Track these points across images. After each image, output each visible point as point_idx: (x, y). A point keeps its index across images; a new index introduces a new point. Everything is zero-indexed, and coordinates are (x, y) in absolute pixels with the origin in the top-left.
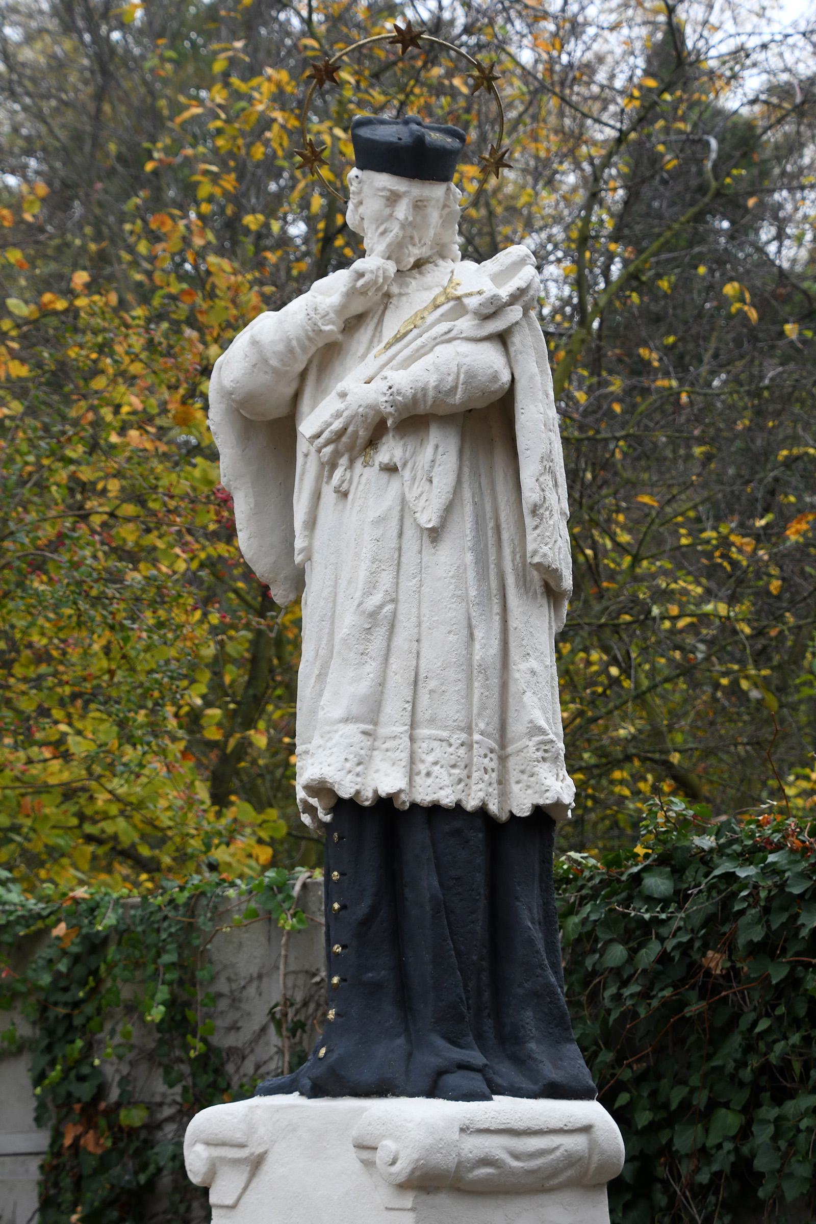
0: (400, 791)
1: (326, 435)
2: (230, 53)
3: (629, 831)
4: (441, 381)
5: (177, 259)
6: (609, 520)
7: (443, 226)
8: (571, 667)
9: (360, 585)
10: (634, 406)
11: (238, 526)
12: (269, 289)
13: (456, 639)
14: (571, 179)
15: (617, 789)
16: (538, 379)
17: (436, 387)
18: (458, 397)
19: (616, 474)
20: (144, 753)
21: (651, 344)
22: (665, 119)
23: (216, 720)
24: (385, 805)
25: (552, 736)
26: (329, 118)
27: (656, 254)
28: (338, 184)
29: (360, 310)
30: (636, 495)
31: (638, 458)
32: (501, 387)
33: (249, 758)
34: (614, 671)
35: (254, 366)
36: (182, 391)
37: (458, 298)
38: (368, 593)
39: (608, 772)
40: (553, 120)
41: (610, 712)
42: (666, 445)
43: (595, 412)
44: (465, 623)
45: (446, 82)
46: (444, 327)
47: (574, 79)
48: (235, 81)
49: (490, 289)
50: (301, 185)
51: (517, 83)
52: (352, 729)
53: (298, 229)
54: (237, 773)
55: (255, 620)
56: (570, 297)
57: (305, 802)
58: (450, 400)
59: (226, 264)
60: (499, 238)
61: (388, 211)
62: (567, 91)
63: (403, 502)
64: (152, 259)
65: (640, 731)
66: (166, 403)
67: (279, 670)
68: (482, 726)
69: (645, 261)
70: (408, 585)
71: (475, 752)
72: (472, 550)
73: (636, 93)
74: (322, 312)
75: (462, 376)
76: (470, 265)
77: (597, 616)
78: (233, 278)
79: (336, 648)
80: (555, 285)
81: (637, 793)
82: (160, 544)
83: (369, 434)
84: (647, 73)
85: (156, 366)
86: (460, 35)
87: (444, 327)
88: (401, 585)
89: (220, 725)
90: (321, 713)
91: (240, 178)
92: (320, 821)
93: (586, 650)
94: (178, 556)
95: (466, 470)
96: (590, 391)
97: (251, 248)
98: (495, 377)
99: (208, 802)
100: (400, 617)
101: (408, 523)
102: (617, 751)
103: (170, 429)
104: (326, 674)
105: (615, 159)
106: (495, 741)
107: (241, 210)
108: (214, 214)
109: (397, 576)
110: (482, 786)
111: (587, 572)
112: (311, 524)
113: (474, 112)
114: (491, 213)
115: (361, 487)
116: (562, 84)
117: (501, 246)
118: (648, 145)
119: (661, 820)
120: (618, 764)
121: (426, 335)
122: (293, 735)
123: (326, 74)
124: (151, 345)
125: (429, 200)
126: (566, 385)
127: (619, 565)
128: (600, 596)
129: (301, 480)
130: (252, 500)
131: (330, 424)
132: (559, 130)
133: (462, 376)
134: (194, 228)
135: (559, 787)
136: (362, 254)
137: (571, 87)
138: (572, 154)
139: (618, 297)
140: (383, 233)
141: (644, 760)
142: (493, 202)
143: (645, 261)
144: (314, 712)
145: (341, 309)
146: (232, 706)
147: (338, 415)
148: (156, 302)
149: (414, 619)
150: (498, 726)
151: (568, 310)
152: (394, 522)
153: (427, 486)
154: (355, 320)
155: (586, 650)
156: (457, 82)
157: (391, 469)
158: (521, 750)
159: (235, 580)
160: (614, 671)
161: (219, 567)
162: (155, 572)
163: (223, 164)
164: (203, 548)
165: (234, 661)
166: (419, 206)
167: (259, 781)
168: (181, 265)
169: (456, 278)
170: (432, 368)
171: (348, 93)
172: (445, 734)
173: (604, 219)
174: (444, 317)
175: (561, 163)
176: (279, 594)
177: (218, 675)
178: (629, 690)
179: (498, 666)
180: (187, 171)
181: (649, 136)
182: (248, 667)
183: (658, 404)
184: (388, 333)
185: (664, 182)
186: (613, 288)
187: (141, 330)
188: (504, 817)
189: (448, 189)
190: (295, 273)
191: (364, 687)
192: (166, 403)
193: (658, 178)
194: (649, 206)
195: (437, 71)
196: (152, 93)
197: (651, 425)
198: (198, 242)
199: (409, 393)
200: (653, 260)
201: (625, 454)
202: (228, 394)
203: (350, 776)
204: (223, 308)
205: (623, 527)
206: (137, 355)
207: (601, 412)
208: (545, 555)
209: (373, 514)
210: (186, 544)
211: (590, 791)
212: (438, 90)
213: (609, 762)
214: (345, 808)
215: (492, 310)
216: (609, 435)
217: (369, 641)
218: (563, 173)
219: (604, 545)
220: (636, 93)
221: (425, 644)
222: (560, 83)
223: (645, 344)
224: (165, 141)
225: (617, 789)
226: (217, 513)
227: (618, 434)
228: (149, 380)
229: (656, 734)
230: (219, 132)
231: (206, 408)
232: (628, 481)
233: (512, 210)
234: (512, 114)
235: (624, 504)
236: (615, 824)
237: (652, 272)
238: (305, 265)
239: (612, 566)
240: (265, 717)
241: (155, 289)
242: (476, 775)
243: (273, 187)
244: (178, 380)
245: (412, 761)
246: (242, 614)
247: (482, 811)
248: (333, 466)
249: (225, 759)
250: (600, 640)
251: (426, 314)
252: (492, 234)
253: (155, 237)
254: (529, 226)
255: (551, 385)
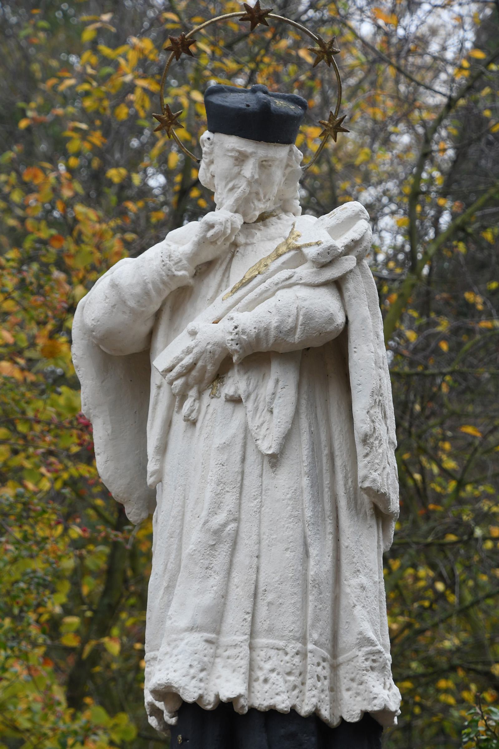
0: (240, 696)
1: (177, 369)
2: (98, 25)
3: (455, 738)
4: (282, 322)
5: (48, 206)
6: (436, 448)
7: (285, 183)
8: (401, 583)
9: (206, 506)
10: (460, 345)
11: (96, 450)
12: (130, 236)
13: (292, 556)
14: (406, 139)
15: (443, 697)
16: (370, 321)
17: (277, 327)
18: (297, 337)
19: (442, 405)
20: (7, 658)
21: (475, 289)
22: (491, 87)
23: (74, 628)
24: (226, 708)
25: (379, 647)
26: (187, 82)
27: (481, 208)
28: (194, 142)
29: (210, 258)
30: (461, 425)
31: (463, 392)
32: (336, 329)
33: (102, 663)
34: (440, 586)
35: (113, 306)
36: (49, 327)
37: (299, 248)
38: (213, 512)
39: (435, 681)
40: (390, 85)
41: (435, 626)
42: (489, 380)
43: (424, 350)
44: (301, 541)
45: (293, 53)
46: (285, 274)
47: (409, 51)
48: (105, 50)
49: (327, 240)
50: (160, 144)
51: (357, 52)
52: (197, 638)
53: (157, 181)
54: (92, 676)
55: (113, 534)
56: (403, 246)
57: (152, 705)
58: (290, 340)
59: (92, 215)
60: (338, 192)
61: (236, 170)
62: (402, 62)
63: (246, 430)
64: (24, 207)
65: (464, 643)
66: (34, 337)
67: (132, 581)
68: (315, 636)
69: (471, 215)
70: (249, 505)
71: (309, 660)
72: (309, 474)
73: (466, 64)
74: (175, 259)
75: (301, 318)
76: (310, 219)
77: (422, 535)
78: (98, 226)
79: (183, 563)
80: (390, 234)
81: (461, 701)
82: (28, 464)
83: (216, 369)
84: (477, 46)
85: (25, 303)
86: (306, 12)
87: (285, 274)
88: (244, 506)
89: (77, 632)
90: (168, 623)
91: (106, 134)
92: (165, 724)
93: (414, 566)
94: (43, 475)
95: (303, 402)
96: (419, 330)
97: (113, 199)
98: (331, 319)
99: (64, 704)
100: (242, 535)
101: (250, 449)
102: (443, 661)
103: (37, 361)
104: (174, 587)
105: (446, 122)
106: (327, 650)
107: (106, 164)
108: (81, 167)
109: (240, 498)
110: (315, 692)
111: (414, 495)
112: (163, 449)
113: (318, 80)
114: (332, 170)
115: (208, 416)
116: (398, 55)
117: (340, 199)
118: (475, 111)
119: (481, 728)
120: (443, 673)
121: (269, 281)
122: (142, 640)
123: (182, 47)
124: (22, 285)
125: (273, 160)
126: (397, 324)
127: (444, 488)
128: (428, 517)
129: (154, 409)
130: (109, 427)
131: (182, 360)
132: (396, 96)
133: (301, 318)
134: (64, 181)
135: (386, 695)
136: (213, 207)
137: (406, 59)
138: (405, 117)
139: (446, 247)
140: (232, 189)
141: (468, 670)
142: (334, 160)
143: (471, 215)
144: (161, 621)
145: (194, 255)
146: (89, 614)
147: (189, 351)
148: (28, 244)
149: (255, 537)
150: (330, 637)
151: (401, 257)
152: (237, 449)
153: (268, 416)
154: (206, 265)
155: (414, 566)
156: (302, 53)
157: (236, 401)
158: (351, 660)
159: (93, 496)
160: (440, 586)
161: (80, 485)
162: (21, 490)
163: (91, 123)
164: (66, 468)
165: (91, 573)
166: (264, 165)
167: (112, 684)
168: (49, 212)
169: (297, 230)
170: (274, 311)
171: (204, 61)
172: (281, 643)
173: (433, 174)
174: (285, 265)
175: (396, 125)
176: (133, 513)
177: (76, 585)
178: (452, 605)
179: (331, 581)
180: (57, 128)
181: (476, 102)
182: (104, 577)
183: (481, 343)
184: (235, 277)
185: (489, 143)
186: (441, 239)
187: (14, 271)
188: (335, 722)
189: (291, 150)
190: (154, 220)
191: (208, 599)
192: (34, 337)
193: (483, 140)
194: (477, 165)
195: (284, 43)
196: (27, 59)
197: (475, 362)
198: (67, 193)
199: (253, 332)
200: (479, 214)
201: (451, 389)
202: (89, 332)
203: (194, 681)
204: (87, 254)
205: (450, 455)
206: (9, 294)
207: (429, 350)
208: (374, 481)
209: (218, 441)
210: (51, 464)
211: (417, 699)
212: (285, 58)
213: (435, 671)
214: (189, 711)
215: (328, 259)
216: (436, 371)
217: (213, 556)
218: (397, 134)
219: (431, 470)
220: (466, 64)
221: (264, 561)
222: (395, 55)
223: (470, 289)
224: (38, 100)
225: (443, 697)
226: (79, 437)
227: (445, 370)
228: (19, 317)
229: (479, 646)
230: (87, 94)
231: (70, 342)
232: (453, 413)
233: (351, 167)
234: (352, 81)
235: (449, 434)
236: (442, 731)
237: (477, 225)
238: (164, 213)
239: (438, 489)
240: (119, 623)
241: (26, 233)
242: (309, 682)
243: (135, 143)
244: (47, 316)
245: (251, 668)
246: (101, 528)
247: (315, 716)
248: (183, 397)
249: (80, 664)
250: (427, 558)
251: (269, 262)
252: (333, 188)
253: (28, 189)
254: (367, 181)
255: (381, 327)
